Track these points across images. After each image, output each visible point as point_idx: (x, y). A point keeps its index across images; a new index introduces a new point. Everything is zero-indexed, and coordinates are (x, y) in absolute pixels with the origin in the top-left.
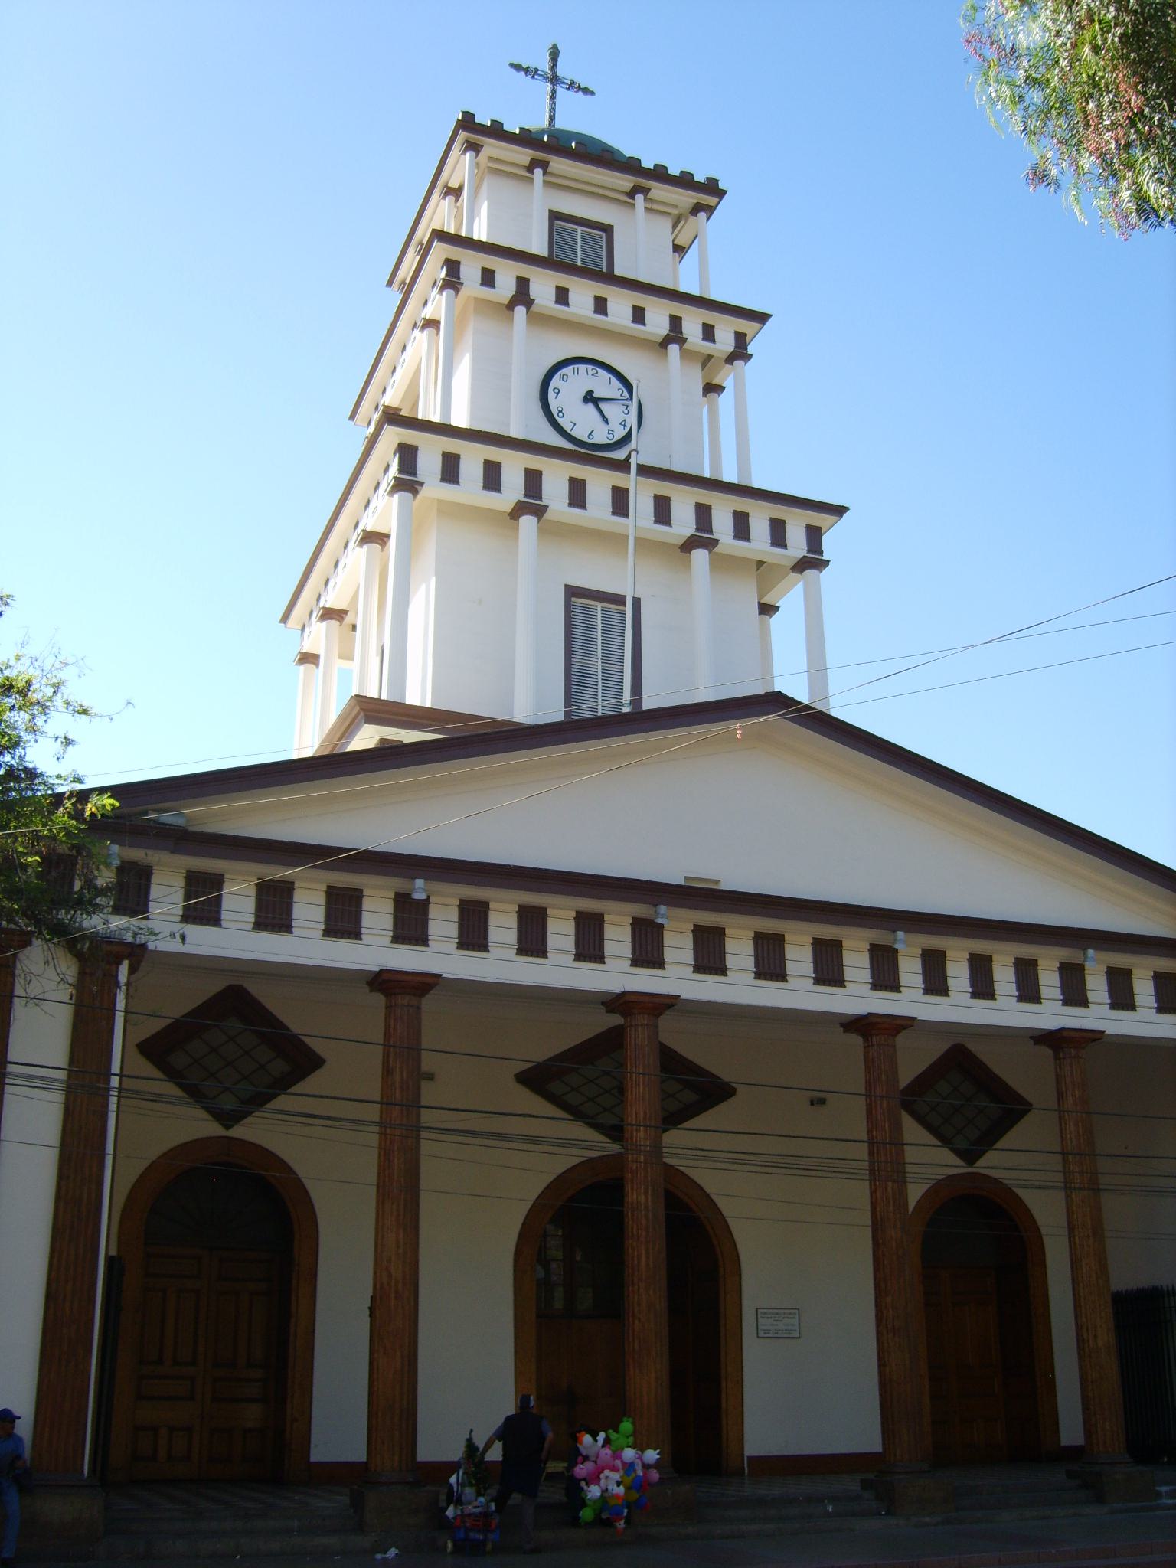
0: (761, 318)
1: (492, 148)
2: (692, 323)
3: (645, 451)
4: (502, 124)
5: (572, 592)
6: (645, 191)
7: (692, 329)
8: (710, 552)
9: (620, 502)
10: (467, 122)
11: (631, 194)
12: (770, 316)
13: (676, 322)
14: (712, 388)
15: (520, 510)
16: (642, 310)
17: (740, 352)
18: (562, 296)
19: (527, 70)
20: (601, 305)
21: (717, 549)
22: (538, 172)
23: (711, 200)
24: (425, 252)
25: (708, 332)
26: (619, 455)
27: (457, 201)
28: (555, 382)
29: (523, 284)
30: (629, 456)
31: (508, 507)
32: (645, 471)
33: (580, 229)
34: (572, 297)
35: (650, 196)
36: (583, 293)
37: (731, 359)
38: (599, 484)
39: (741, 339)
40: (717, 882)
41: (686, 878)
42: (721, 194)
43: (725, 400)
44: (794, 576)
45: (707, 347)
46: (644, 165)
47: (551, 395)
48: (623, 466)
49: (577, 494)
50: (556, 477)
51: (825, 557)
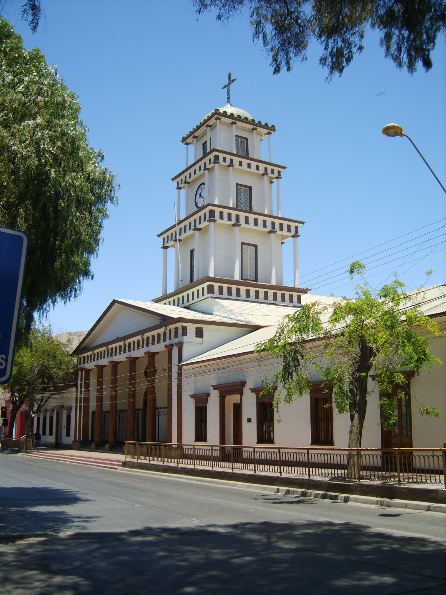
0: (284, 168)
17: (279, 177)
36: (245, 162)
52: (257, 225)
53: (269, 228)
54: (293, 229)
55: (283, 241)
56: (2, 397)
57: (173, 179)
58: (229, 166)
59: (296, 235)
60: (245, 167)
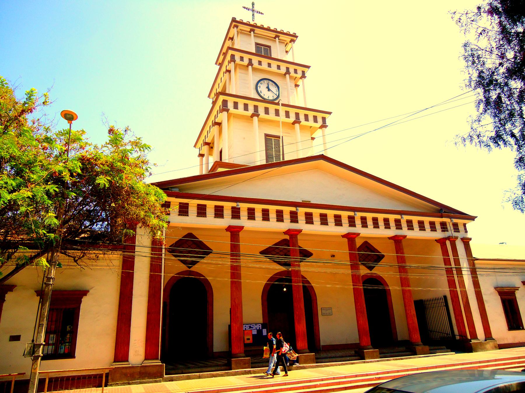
0: (308, 67)
1: (241, 27)
2: (292, 68)
3: (283, 100)
4: (236, 18)
5: (266, 135)
6: (278, 37)
7: (292, 71)
8: (258, 117)
9: (277, 113)
10: (234, 20)
11: (275, 38)
12: (310, 66)
13: (288, 69)
14: (297, 86)
15: (253, 116)
16: (270, 64)
17: (303, 76)
18: (260, 63)
19: (247, 8)
20: (269, 65)
21: (301, 124)
22: (252, 33)
23: (295, 39)
24: (225, 54)
25: (242, 59)
26: (277, 101)
27: (232, 41)
28: (259, 85)
29: (250, 60)
30: (279, 101)
31: (250, 115)
32: (283, 105)
33: (263, 47)
34: (272, 65)
35: (279, 38)
36: (265, 61)
37: (301, 78)
38: (272, 108)
39: (303, 72)
40: (310, 201)
41: (302, 201)
42: (297, 37)
43: (300, 89)
44: (319, 129)
45: (295, 75)
46: (237, 19)
47: (258, 88)
48: (278, 104)
49: (267, 111)
50: (262, 106)
51: (327, 125)
52: (268, 114)
53: (292, 118)
54: (320, 120)
55: (313, 136)
56: (524, 148)
57: (195, 146)
58: (294, 123)
59: (324, 126)
60: (265, 66)
